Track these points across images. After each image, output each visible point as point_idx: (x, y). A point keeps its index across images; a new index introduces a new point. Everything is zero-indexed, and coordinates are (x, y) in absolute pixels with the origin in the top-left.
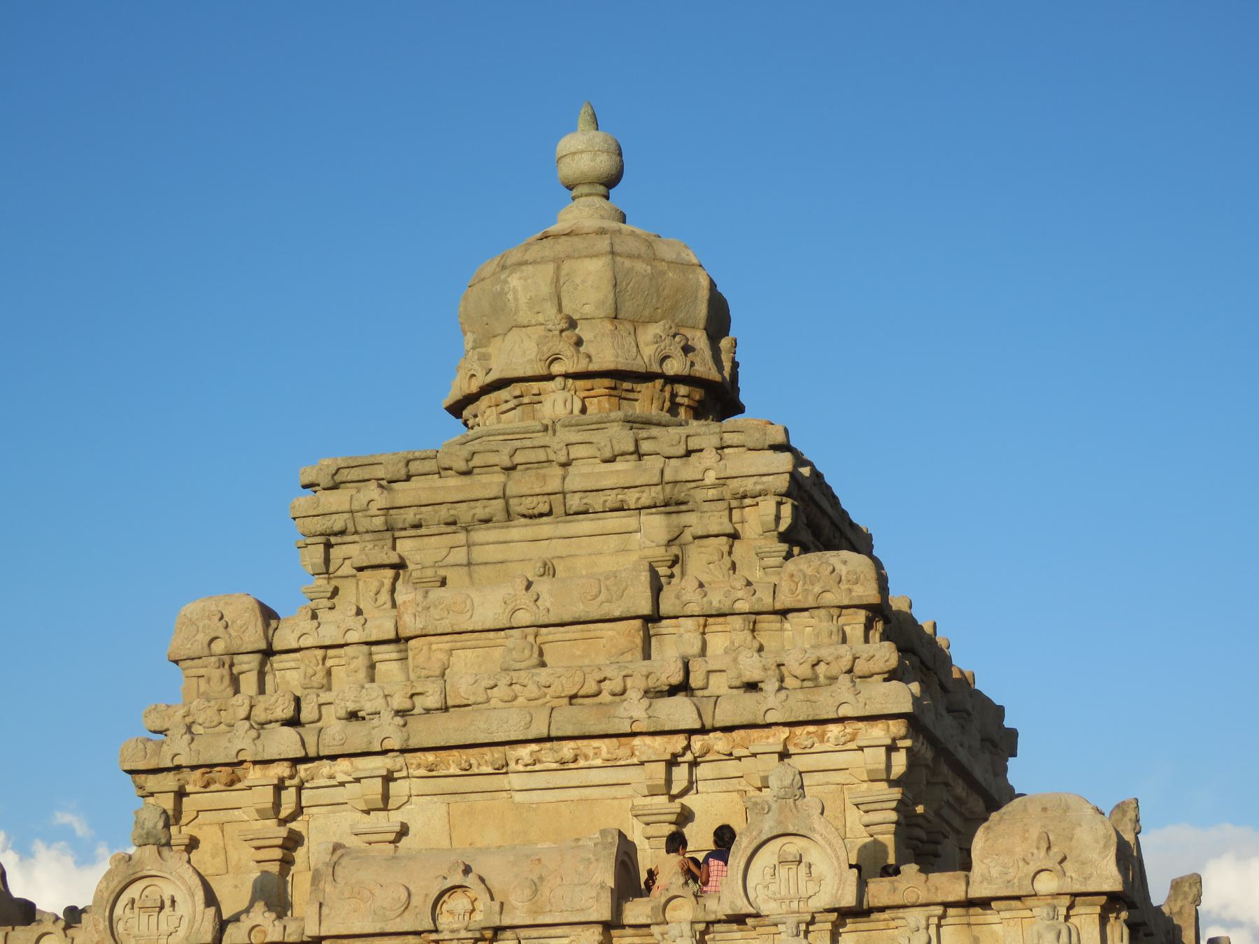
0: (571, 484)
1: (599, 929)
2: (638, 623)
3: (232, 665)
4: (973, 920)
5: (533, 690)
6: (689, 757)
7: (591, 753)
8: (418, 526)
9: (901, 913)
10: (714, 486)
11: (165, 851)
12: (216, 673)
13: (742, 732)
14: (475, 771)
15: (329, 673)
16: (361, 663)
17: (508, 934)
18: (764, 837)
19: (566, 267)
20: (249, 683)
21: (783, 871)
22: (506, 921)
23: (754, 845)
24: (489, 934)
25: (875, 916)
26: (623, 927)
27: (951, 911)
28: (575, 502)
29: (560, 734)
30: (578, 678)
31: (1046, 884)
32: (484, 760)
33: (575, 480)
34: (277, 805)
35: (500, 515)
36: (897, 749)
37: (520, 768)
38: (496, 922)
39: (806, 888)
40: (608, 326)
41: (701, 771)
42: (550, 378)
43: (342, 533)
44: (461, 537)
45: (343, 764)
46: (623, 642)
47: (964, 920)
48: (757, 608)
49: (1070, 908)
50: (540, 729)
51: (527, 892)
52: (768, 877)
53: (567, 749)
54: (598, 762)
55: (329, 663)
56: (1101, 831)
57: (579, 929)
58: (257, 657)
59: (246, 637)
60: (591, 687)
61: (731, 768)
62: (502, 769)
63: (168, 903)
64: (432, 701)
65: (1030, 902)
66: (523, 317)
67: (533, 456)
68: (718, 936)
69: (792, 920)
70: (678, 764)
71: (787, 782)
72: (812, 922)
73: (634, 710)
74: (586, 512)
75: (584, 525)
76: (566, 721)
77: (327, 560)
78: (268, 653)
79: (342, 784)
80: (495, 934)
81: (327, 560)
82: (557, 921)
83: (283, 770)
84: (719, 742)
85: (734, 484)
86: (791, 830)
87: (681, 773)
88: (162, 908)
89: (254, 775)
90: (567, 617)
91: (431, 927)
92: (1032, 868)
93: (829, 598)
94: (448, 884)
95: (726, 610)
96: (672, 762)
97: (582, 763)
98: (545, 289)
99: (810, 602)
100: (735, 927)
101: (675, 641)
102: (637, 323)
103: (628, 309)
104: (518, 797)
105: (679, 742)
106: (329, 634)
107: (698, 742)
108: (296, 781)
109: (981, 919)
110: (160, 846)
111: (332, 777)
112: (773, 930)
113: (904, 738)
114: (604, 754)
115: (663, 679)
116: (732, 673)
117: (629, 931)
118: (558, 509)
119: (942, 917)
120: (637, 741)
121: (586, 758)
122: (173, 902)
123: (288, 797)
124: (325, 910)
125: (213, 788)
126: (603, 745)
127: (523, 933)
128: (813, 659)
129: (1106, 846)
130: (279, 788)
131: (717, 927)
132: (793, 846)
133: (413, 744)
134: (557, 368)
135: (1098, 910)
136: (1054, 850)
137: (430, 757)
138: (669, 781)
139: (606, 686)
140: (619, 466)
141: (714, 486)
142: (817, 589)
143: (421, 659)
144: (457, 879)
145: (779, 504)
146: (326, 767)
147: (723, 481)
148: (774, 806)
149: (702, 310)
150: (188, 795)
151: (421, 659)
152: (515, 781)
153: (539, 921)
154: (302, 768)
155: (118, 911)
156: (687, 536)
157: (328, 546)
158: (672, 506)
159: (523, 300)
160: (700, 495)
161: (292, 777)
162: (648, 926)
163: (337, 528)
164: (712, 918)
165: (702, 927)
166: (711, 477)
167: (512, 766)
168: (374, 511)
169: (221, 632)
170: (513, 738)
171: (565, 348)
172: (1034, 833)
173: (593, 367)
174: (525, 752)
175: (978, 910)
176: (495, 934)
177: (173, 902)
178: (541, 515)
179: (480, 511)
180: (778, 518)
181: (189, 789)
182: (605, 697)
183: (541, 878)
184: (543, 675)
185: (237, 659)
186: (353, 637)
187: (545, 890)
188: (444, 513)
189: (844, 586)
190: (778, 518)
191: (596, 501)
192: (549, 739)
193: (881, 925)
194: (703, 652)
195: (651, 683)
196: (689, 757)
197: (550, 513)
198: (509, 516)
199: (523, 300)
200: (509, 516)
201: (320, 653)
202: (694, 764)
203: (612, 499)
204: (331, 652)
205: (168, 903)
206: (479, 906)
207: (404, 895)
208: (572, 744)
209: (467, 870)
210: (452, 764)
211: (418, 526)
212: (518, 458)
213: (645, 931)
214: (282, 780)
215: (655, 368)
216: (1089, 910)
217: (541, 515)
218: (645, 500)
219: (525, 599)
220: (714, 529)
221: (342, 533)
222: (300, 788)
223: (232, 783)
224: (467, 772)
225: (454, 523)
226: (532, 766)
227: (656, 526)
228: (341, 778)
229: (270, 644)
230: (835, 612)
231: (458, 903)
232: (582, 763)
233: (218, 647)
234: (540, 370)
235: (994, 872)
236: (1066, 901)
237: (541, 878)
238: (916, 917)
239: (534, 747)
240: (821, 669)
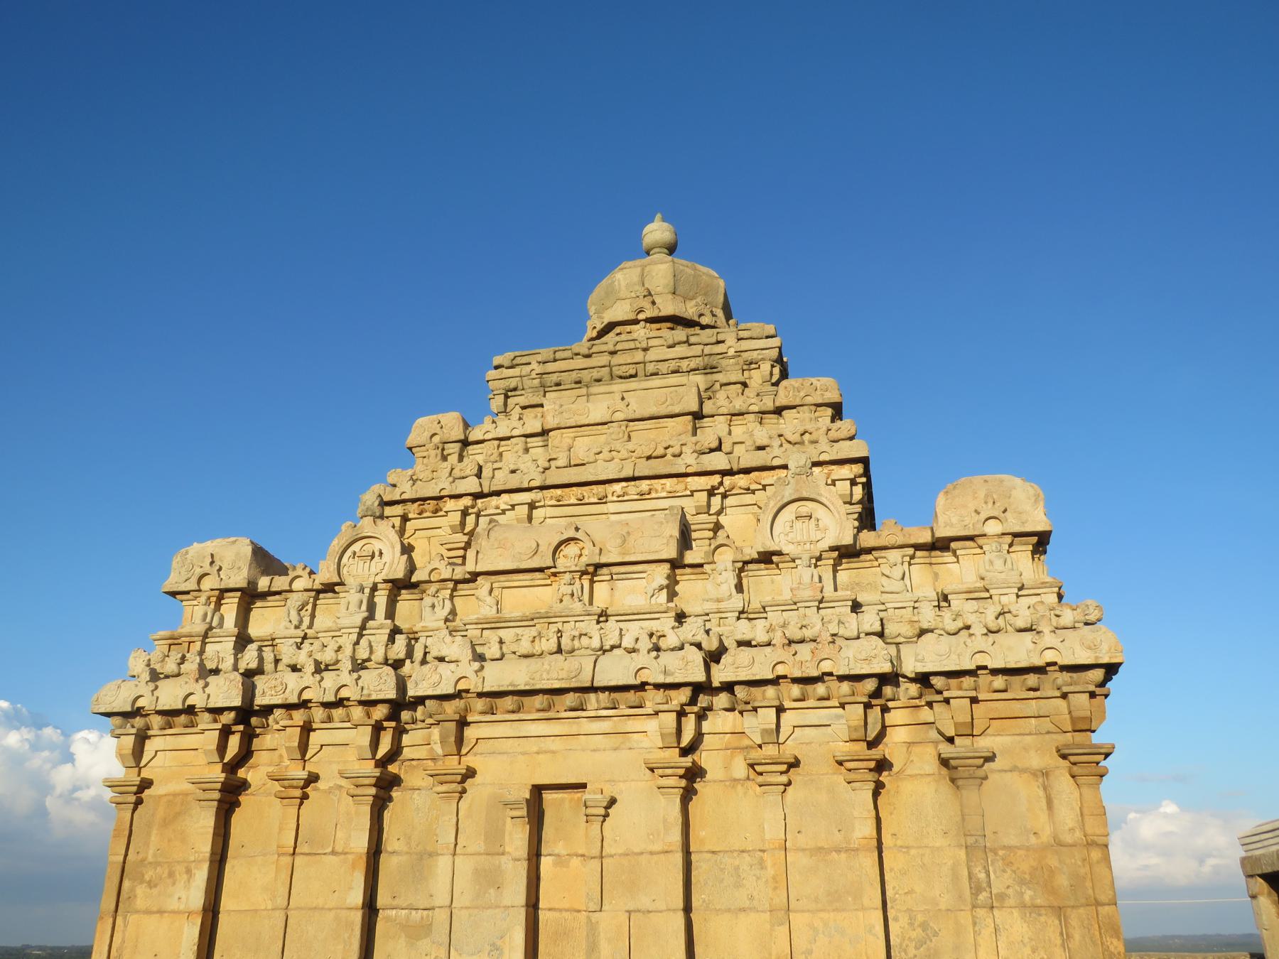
0: (648, 358)
1: (667, 566)
2: (690, 417)
3: (443, 449)
4: (934, 560)
5: (624, 454)
6: (722, 490)
7: (659, 488)
8: (558, 384)
9: (883, 553)
10: (733, 357)
11: (378, 521)
12: (433, 453)
13: (756, 473)
14: (586, 501)
15: (501, 455)
16: (520, 447)
17: (605, 570)
18: (785, 500)
19: (647, 269)
20: (453, 459)
21: (798, 524)
22: (604, 560)
23: (779, 505)
24: (591, 569)
25: (863, 557)
26: (684, 566)
27: (919, 553)
28: (651, 368)
29: (641, 474)
30: (653, 445)
31: (993, 528)
32: (591, 494)
33: (652, 355)
34: (463, 524)
35: (607, 377)
36: (856, 484)
37: (615, 498)
38: (596, 560)
39: (815, 535)
40: (670, 296)
41: (729, 501)
42: (636, 322)
43: (515, 389)
44: (584, 391)
45: (505, 497)
46: (680, 428)
47: (927, 560)
48: (764, 409)
49: (1011, 545)
50: (628, 472)
51: (619, 541)
52: (788, 529)
53: (644, 485)
54: (664, 494)
55: (501, 449)
56: (1032, 492)
57: (654, 565)
58: (458, 445)
59: (453, 433)
60: (660, 451)
61: (749, 498)
62: (602, 500)
63: (377, 553)
64: (561, 463)
65: (980, 541)
66: (622, 295)
67: (627, 345)
68: (751, 573)
69: (806, 557)
70: (715, 495)
71: (802, 463)
72: (819, 559)
73: (689, 461)
74: (657, 374)
75: (656, 382)
76: (645, 468)
77: (505, 404)
78: (465, 443)
79: (504, 512)
80: (596, 570)
81: (505, 404)
82: (639, 559)
83: (467, 501)
84: (741, 480)
85: (745, 355)
86: (805, 495)
87: (716, 501)
88: (373, 557)
89: (450, 505)
90: (646, 415)
91: (550, 563)
92: (983, 516)
93: (809, 400)
94: (565, 537)
95: (744, 410)
96: (711, 493)
97: (653, 495)
98: (636, 279)
99: (798, 402)
100: (763, 566)
101: (712, 430)
102: (686, 299)
103: (680, 290)
104: (613, 517)
105: (716, 479)
106: (502, 431)
107: (728, 481)
108: (475, 510)
109: (940, 560)
110: (375, 517)
111: (497, 508)
112: (792, 565)
113: (860, 476)
114: (668, 488)
115: (706, 445)
116: (749, 443)
117: (688, 570)
118: (641, 373)
119: (912, 557)
120: (689, 479)
121: (657, 491)
122: (381, 554)
123: (470, 520)
124: (480, 556)
125: (425, 515)
126: (668, 482)
127: (615, 569)
128: (802, 430)
129: (1036, 501)
130: (465, 513)
131: (751, 566)
132: (806, 507)
133: (549, 482)
134: (641, 316)
135: (1031, 548)
136: (998, 504)
137: (559, 492)
138: (709, 505)
139: (670, 451)
140: (678, 348)
141: (733, 357)
142: (802, 394)
143: (556, 442)
144: (572, 534)
145: (773, 366)
146: (494, 501)
147: (739, 353)
148: (792, 481)
149: (721, 299)
150: (468, 724)
151: (556, 442)
152: (612, 507)
153: (627, 559)
154: (479, 501)
155: (345, 560)
156: (717, 386)
157: (507, 397)
158: (710, 369)
159: (623, 284)
160: (724, 362)
161: (473, 507)
162: (701, 565)
163: (512, 386)
164: (747, 558)
165: (740, 565)
166: (731, 352)
167: (610, 498)
168: (534, 375)
169: (438, 430)
170: (611, 477)
171: (646, 304)
172: (982, 494)
173: (663, 314)
174: (617, 487)
175: (938, 553)
176: (596, 570)
177: (381, 554)
178: (631, 376)
179: (596, 374)
180: (771, 374)
181: (410, 516)
182: (669, 457)
183: (628, 533)
184: (630, 446)
185: (446, 446)
186: (515, 433)
187: (631, 540)
188: (574, 375)
189: (819, 392)
190: (771, 374)
191: (663, 367)
192: (634, 479)
193: (867, 564)
194: (730, 433)
195: (698, 448)
196: (722, 490)
197: (635, 376)
198: (612, 378)
199: (623, 284)
200: (612, 378)
201: (496, 442)
202: (724, 496)
203: (673, 365)
204: (503, 443)
205: (377, 553)
206: (585, 552)
207: (534, 545)
208: (648, 482)
209: (577, 529)
210: (572, 495)
211: (558, 384)
212: (619, 347)
213: (699, 570)
214: (467, 508)
215: (696, 318)
216: (1024, 548)
217: (631, 376)
218: (693, 365)
219: (621, 405)
220: (733, 379)
221: (515, 389)
222: (478, 515)
223: (436, 511)
224: (581, 502)
225: (579, 382)
226: (622, 498)
227: (700, 380)
228: (503, 507)
229: (467, 438)
230: (813, 408)
231: (571, 550)
232: (653, 495)
233: (436, 439)
234: (631, 316)
235: (954, 520)
236: (1008, 539)
237: (628, 533)
238: (894, 555)
239: (624, 484)
240: (807, 437)
